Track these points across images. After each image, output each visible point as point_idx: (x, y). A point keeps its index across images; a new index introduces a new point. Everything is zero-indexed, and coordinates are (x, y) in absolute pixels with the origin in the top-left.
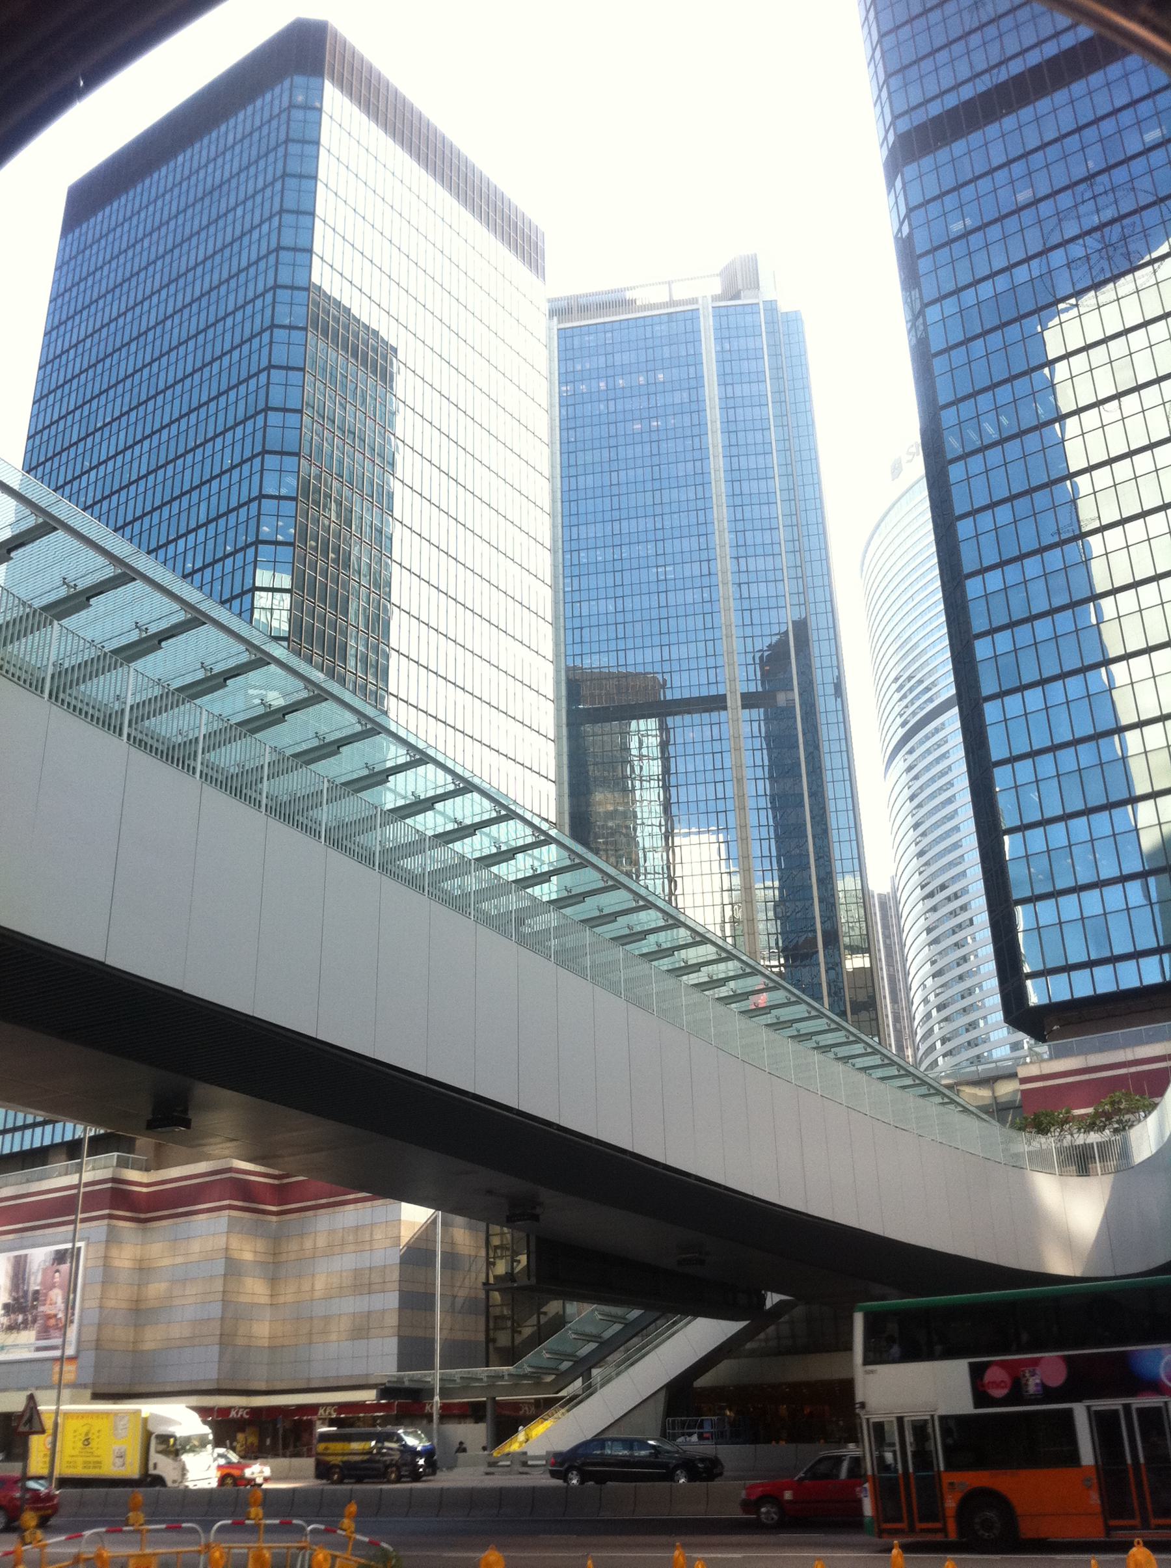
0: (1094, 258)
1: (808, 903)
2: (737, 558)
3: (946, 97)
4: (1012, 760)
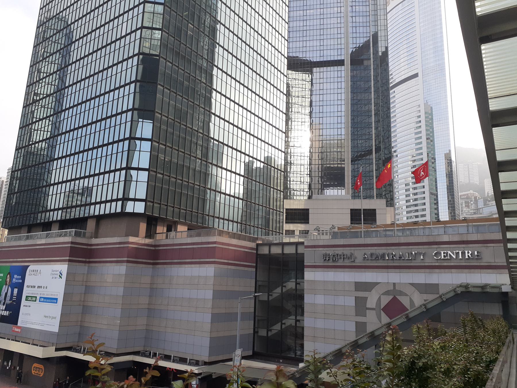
1: (371, 178)
2: (352, 6)
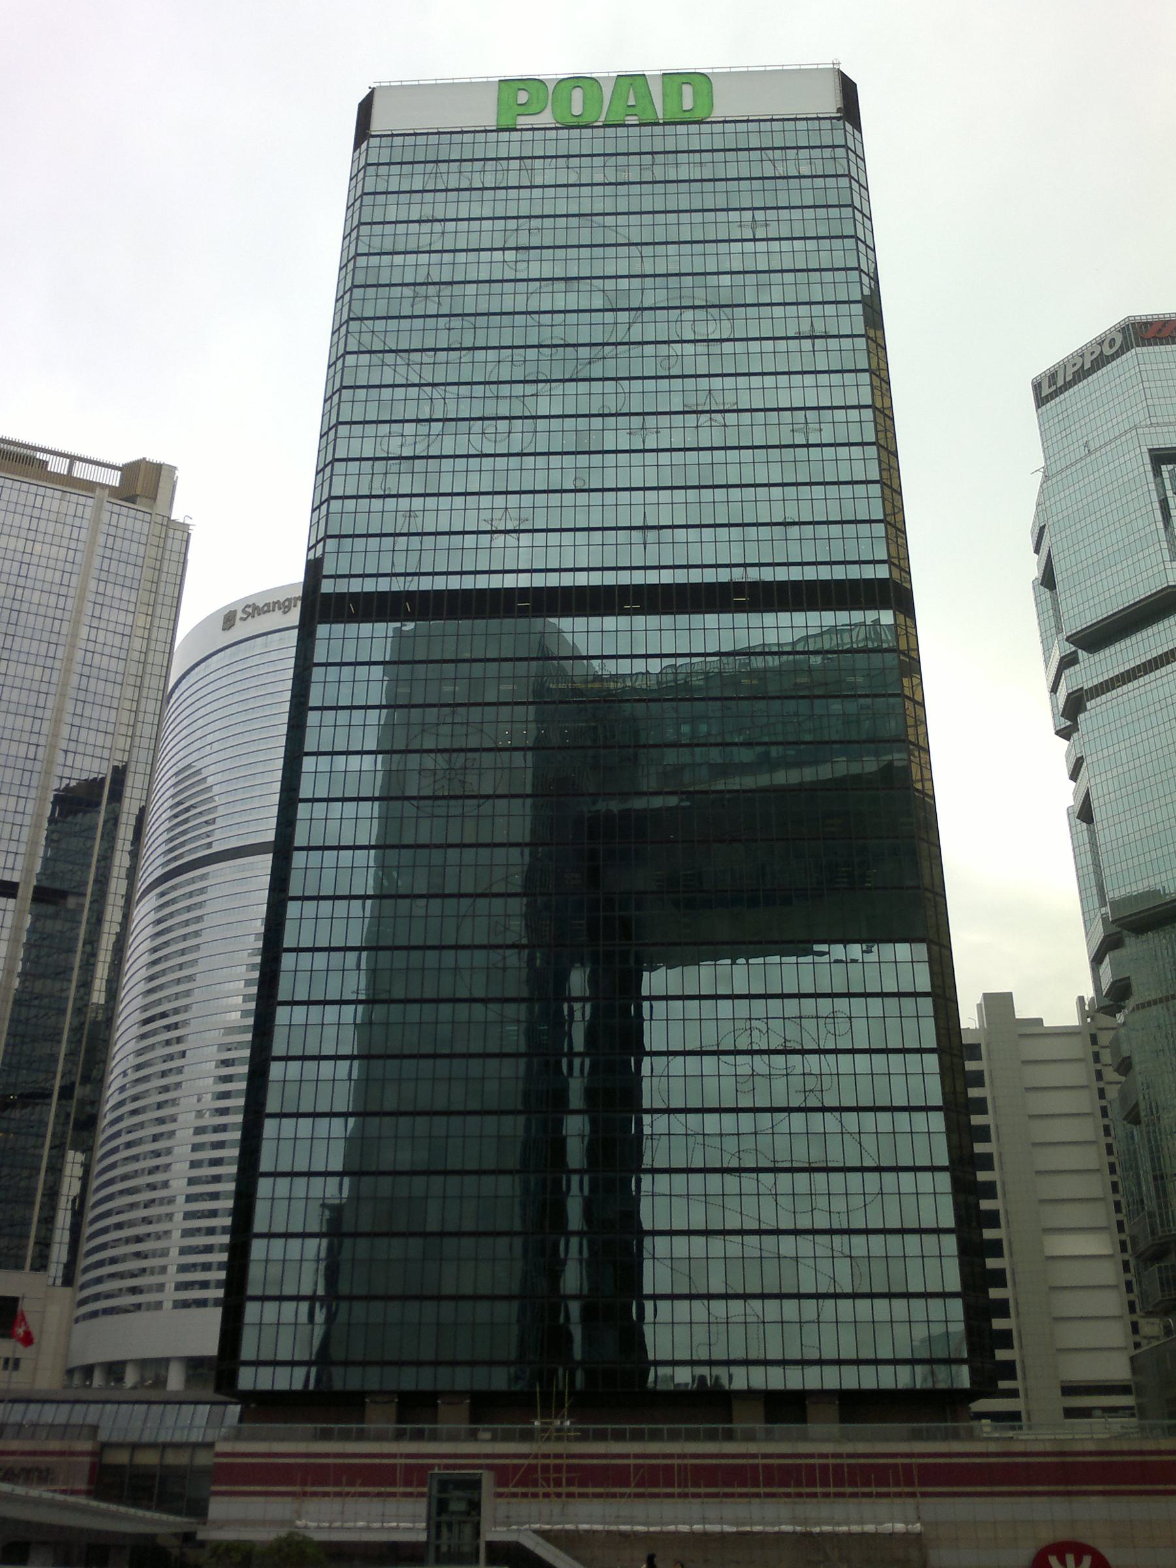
0: (440, 774)
1: (51, 1075)
4: (275, 1175)
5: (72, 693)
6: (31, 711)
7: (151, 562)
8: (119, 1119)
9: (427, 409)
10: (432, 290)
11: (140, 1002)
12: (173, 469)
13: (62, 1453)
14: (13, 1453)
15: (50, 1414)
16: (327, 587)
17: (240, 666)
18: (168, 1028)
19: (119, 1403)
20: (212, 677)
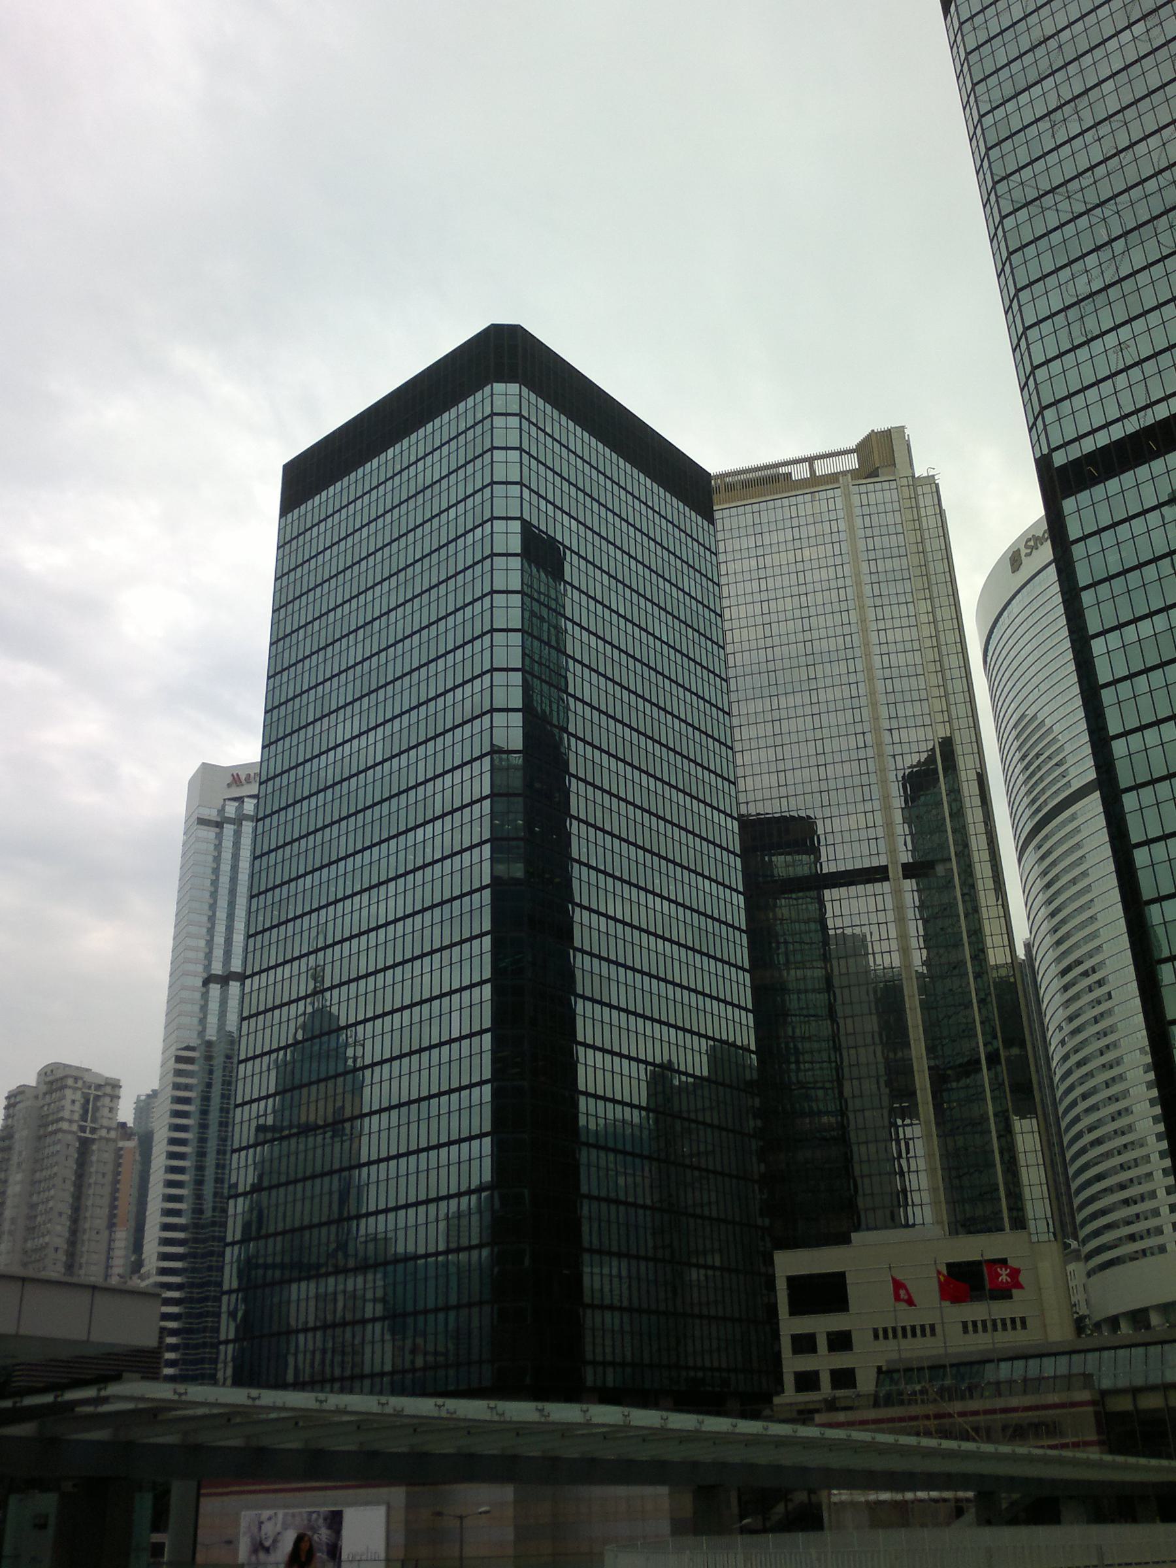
3: (1098, 435)
5: (879, 673)
6: (848, 703)
7: (910, 525)
8: (1069, 1073)
9: (1103, 232)
10: (1067, 109)
11: (1051, 955)
12: (901, 429)
13: (1062, 1406)
14: (1015, 1410)
15: (1061, 1366)
16: (1059, 459)
17: (1036, 604)
18: (1086, 974)
19: (1116, 1348)
20: (1018, 621)
